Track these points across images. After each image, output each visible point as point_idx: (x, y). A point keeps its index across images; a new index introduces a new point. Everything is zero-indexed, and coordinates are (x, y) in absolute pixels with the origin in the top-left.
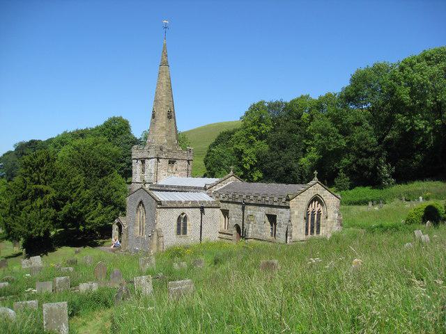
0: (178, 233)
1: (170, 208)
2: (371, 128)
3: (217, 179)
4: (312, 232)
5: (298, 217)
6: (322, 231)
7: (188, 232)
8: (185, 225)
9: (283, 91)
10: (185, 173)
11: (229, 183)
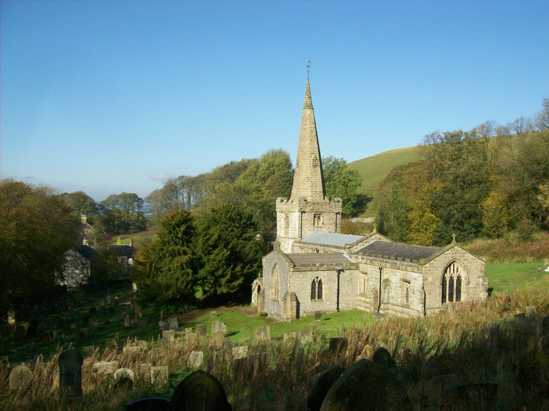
0: (313, 297)
1: (304, 271)
2: (152, 292)
3: (358, 238)
4: (451, 299)
5: (432, 283)
6: (464, 297)
7: (324, 296)
8: (320, 288)
9: (463, 121)
10: (333, 227)
11: (372, 242)
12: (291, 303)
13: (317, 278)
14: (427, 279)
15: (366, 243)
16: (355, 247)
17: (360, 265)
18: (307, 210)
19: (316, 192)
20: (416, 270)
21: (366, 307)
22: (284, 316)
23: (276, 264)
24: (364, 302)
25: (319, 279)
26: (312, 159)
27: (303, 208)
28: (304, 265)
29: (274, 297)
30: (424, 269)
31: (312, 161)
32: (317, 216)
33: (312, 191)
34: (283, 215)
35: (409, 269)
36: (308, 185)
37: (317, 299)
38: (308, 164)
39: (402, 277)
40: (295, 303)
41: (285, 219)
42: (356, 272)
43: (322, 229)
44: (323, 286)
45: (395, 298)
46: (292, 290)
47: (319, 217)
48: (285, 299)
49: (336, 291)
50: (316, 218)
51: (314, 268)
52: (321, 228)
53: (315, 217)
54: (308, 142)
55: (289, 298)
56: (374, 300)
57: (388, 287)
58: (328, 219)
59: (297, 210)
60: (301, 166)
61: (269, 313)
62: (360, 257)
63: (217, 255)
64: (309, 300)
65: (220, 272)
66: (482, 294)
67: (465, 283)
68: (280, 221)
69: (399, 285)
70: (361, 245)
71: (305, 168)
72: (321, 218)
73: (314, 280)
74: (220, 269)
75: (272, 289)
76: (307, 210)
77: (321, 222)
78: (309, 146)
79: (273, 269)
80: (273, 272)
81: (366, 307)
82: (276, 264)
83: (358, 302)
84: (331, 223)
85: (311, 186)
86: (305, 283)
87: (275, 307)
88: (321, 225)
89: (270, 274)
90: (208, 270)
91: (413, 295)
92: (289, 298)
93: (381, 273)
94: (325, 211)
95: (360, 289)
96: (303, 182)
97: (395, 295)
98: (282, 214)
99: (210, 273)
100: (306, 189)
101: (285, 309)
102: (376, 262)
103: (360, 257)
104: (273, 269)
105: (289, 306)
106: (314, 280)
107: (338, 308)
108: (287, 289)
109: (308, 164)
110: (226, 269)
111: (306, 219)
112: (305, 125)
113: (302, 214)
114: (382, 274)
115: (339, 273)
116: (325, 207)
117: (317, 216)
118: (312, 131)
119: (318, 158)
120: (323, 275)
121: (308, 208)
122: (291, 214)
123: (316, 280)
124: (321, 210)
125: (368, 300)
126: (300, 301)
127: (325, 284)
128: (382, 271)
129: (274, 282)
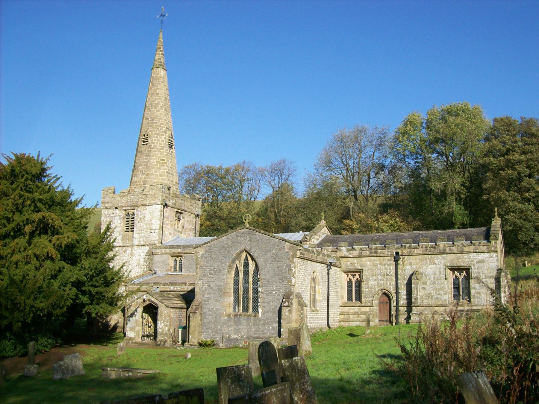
20: (484, 248)
24: (355, 314)
27: (166, 199)
32: (179, 213)
35: (467, 249)
36: (162, 170)
38: (163, 141)
39: (449, 264)
52: (181, 233)
58: (188, 221)
61: (218, 339)
71: (158, 146)
75: (230, 296)
76: (170, 203)
84: (191, 229)
94: (186, 209)
96: (156, 165)
97: (433, 292)
100: (161, 176)
107: (328, 325)
109: (163, 141)
111: (168, 218)
112: (158, 89)
114: (400, 267)
117: (179, 213)
118: (166, 98)
121: (171, 201)
122: (141, 208)
128: (400, 262)
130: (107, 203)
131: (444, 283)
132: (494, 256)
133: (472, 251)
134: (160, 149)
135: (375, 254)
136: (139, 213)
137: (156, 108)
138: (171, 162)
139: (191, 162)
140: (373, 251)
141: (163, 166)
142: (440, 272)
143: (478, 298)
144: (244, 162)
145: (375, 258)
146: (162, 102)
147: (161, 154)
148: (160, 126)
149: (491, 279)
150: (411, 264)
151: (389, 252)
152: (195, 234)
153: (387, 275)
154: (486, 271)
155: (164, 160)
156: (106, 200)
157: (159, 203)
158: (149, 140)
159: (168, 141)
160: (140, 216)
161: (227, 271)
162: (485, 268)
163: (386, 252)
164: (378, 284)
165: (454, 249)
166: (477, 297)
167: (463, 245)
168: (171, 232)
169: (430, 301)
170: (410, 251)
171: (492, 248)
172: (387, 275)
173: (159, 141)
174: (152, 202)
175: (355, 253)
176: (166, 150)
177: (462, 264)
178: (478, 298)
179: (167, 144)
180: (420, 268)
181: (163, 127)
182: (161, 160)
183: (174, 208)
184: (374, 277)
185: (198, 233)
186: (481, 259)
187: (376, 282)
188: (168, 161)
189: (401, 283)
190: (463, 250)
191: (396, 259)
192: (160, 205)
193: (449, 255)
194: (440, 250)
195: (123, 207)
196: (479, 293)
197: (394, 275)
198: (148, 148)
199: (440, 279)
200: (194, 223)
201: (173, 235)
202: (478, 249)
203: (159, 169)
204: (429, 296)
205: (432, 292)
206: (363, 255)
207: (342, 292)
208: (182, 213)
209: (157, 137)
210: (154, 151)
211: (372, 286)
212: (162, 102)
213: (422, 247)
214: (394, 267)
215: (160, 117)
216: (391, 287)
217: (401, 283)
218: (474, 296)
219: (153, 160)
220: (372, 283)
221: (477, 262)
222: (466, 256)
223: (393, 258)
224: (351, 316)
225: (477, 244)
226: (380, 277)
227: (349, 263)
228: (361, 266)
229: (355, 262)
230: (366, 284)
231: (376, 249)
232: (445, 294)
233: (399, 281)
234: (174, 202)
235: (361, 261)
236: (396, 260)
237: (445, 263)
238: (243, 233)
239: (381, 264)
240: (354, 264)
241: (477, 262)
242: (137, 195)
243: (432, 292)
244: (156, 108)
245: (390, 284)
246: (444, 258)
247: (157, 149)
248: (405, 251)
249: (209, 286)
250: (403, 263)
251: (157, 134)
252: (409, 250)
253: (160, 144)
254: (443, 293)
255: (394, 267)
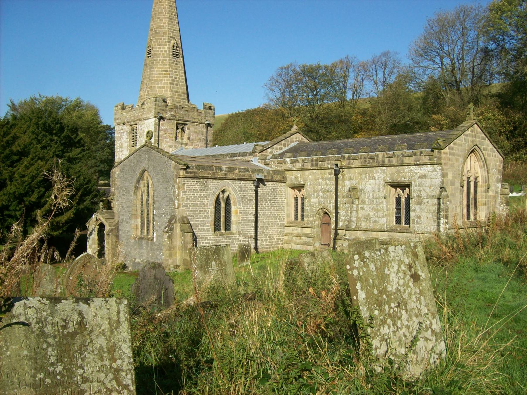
1: (203, 178)
12: (183, 235)
13: (223, 191)
14: (447, 174)
15: (284, 145)
16: (269, 150)
17: (288, 174)
18: (167, 116)
19: (177, 92)
20: (426, 160)
21: (305, 244)
22: (170, 261)
23: (144, 171)
24: (299, 236)
25: (226, 195)
26: (172, 44)
27: (161, 112)
28: (203, 167)
29: (139, 233)
30: (443, 156)
31: (171, 47)
33: (172, 91)
34: (127, 128)
35: (407, 160)
36: (166, 81)
37: (223, 231)
39: (388, 179)
40: (189, 236)
41: (130, 133)
42: (281, 186)
43: (188, 146)
44: (233, 208)
45: (373, 218)
46: (180, 213)
47: (183, 129)
48: (171, 229)
49: (253, 218)
50: (180, 130)
51: (220, 174)
52: (186, 144)
53: (177, 128)
54: (166, 21)
55: (177, 228)
56: (319, 230)
57: (356, 202)
58: (195, 132)
59: (152, 114)
60: (155, 54)
61: (128, 263)
62: (288, 160)
63: (27, 168)
64: (212, 233)
65: (33, 198)
66: (501, 208)
67: (484, 189)
68: (121, 138)
69: (382, 194)
70: (277, 149)
71: (161, 57)
72: (187, 131)
73: (219, 195)
74: (33, 192)
75: (136, 218)
76: (167, 115)
77: (186, 136)
78: (166, 26)
79: (138, 182)
80: (137, 188)
81: (305, 244)
82: (144, 171)
83: (286, 238)
84: (200, 139)
85: (171, 84)
86: (205, 201)
87: (144, 251)
88: (185, 140)
89: (132, 192)
90: (12, 191)
91: (417, 207)
92: (177, 228)
93: (337, 179)
94: (191, 120)
95: (288, 216)
96: (158, 77)
97: (372, 214)
98: (125, 127)
99: (15, 197)
100: (163, 87)
101: (171, 248)
102: (325, 163)
103: (288, 160)
104: (138, 182)
105: (178, 242)
106: (219, 195)
108: (173, 211)
110: (45, 193)
111: (166, 130)
113: (159, 121)
114: (340, 181)
115: (257, 187)
116: (191, 113)
118: (171, 6)
119: (180, 46)
120: (233, 188)
121: (169, 113)
123: (221, 196)
124: (186, 118)
125: (308, 231)
126: (197, 234)
127: (235, 205)
128: (340, 176)
129: (139, 207)
130: (118, 119)
131: (382, 203)
132: (438, 170)
133: (413, 163)
134: (163, 60)
135: (315, 167)
136: (140, 128)
137: (159, 18)
138: (175, 72)
139: (285, 63)
140: (314, 163)
141: (165, 77)
142: (379, 189)
143: (418, 223)
144: (347, 58)
145: (317, 171)
146: (165, 10)
147: (164, 65)
148: (163, 36)
149: (433, 200)
150: (350, 179)
151: (328, 164)
152: (207, 144)
153: (328, 191)
154: (428, 189)
155: (166, 71)
156: (117, 116)
157: (153, 116)
158: (153, 53)
159: (171, 50)
160: (141, 131)
161: (133, 191)
162: (427, 185)
163: (326, 164)
164: (319, 202)
165: (394, 160)
166: (417, 222)
167: (403, 156)
168: (170, 144)
169: (368, 225)
170: (349, 163)
171: (435, 159)
172: (328, 191)
173: (162, 51)
174: (148, 116)
175: (298, 165)
176: (170, 60)
177: (403, 179)
178: (418, 223)
179: (171, 53)
180: (359, 183)
181: (166, 36)
182: (164, 71)
183: (173, 120)
184: (316, 194)
185: (210, 144)
186: (423, 174)
187: (317, 200)
188: (172, 71)
189: (340, 201)
190: (402, 161)
191: (337, 172)
192: (154, 119)
193: (389, 168)
194: (379, 162)
195: (128, 122)
196: (419, 217)
197: (334, 191)
198: (151, 60)
199: (379, 198)
200: (205, 133)
201: (173, 148)
202: (419, 161)
203: (162, 80)
204: (367, 218)
205: (371, 213)
206: (306, 167)
207: (288, 210)
208: (187, 124)
209: (160, 48)
210: (156, 63)
211: (314, 203)
212: (165, 10)
213: (361, 158)
214: (334, 182)
215: (163, 26)
216: (331, 205)
217: (340, 201)
218: (414, 220)
219: (156, 72)
220: (313, 200)
221: (420, 177)
222: (406, 169)
223: (333, 171)
224: (294, 238)
225: (419, 154)
226: (321, 194)
227: (293, 177)
228: (304, 180)
229: (299, 175)
230: (308, 202)
231: (317, 160)
232: (383, 217)
233: (339, 199)
234: (173, 113)
235: (304, 174)
236: (337, 174)
237: (384, 178)
238: (144, 151)
239: (322, 178)
240: (298, 178)
241: (420, 177)
242: (137, 110)
243: (371, 213)
244: (159, 18)
245: (330, 203)
246: (384, 172)
247: (160, 60)
248: (344, 163)
249: (123, 207)
250: (343, 178)
251: (160, 45)
252: (348, 161)
253: (163, 54)
254: (381, 215)
255: (334, 182)
